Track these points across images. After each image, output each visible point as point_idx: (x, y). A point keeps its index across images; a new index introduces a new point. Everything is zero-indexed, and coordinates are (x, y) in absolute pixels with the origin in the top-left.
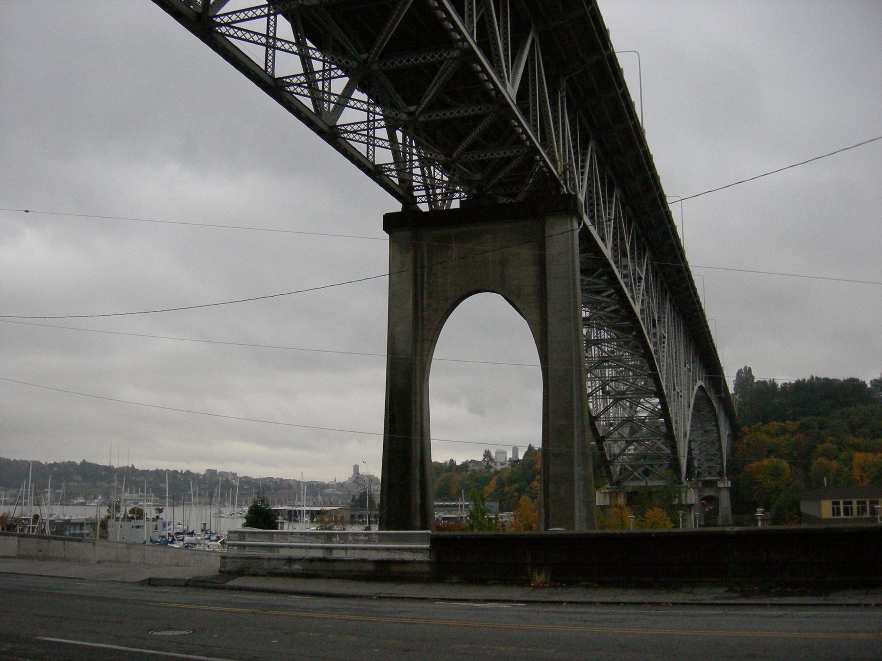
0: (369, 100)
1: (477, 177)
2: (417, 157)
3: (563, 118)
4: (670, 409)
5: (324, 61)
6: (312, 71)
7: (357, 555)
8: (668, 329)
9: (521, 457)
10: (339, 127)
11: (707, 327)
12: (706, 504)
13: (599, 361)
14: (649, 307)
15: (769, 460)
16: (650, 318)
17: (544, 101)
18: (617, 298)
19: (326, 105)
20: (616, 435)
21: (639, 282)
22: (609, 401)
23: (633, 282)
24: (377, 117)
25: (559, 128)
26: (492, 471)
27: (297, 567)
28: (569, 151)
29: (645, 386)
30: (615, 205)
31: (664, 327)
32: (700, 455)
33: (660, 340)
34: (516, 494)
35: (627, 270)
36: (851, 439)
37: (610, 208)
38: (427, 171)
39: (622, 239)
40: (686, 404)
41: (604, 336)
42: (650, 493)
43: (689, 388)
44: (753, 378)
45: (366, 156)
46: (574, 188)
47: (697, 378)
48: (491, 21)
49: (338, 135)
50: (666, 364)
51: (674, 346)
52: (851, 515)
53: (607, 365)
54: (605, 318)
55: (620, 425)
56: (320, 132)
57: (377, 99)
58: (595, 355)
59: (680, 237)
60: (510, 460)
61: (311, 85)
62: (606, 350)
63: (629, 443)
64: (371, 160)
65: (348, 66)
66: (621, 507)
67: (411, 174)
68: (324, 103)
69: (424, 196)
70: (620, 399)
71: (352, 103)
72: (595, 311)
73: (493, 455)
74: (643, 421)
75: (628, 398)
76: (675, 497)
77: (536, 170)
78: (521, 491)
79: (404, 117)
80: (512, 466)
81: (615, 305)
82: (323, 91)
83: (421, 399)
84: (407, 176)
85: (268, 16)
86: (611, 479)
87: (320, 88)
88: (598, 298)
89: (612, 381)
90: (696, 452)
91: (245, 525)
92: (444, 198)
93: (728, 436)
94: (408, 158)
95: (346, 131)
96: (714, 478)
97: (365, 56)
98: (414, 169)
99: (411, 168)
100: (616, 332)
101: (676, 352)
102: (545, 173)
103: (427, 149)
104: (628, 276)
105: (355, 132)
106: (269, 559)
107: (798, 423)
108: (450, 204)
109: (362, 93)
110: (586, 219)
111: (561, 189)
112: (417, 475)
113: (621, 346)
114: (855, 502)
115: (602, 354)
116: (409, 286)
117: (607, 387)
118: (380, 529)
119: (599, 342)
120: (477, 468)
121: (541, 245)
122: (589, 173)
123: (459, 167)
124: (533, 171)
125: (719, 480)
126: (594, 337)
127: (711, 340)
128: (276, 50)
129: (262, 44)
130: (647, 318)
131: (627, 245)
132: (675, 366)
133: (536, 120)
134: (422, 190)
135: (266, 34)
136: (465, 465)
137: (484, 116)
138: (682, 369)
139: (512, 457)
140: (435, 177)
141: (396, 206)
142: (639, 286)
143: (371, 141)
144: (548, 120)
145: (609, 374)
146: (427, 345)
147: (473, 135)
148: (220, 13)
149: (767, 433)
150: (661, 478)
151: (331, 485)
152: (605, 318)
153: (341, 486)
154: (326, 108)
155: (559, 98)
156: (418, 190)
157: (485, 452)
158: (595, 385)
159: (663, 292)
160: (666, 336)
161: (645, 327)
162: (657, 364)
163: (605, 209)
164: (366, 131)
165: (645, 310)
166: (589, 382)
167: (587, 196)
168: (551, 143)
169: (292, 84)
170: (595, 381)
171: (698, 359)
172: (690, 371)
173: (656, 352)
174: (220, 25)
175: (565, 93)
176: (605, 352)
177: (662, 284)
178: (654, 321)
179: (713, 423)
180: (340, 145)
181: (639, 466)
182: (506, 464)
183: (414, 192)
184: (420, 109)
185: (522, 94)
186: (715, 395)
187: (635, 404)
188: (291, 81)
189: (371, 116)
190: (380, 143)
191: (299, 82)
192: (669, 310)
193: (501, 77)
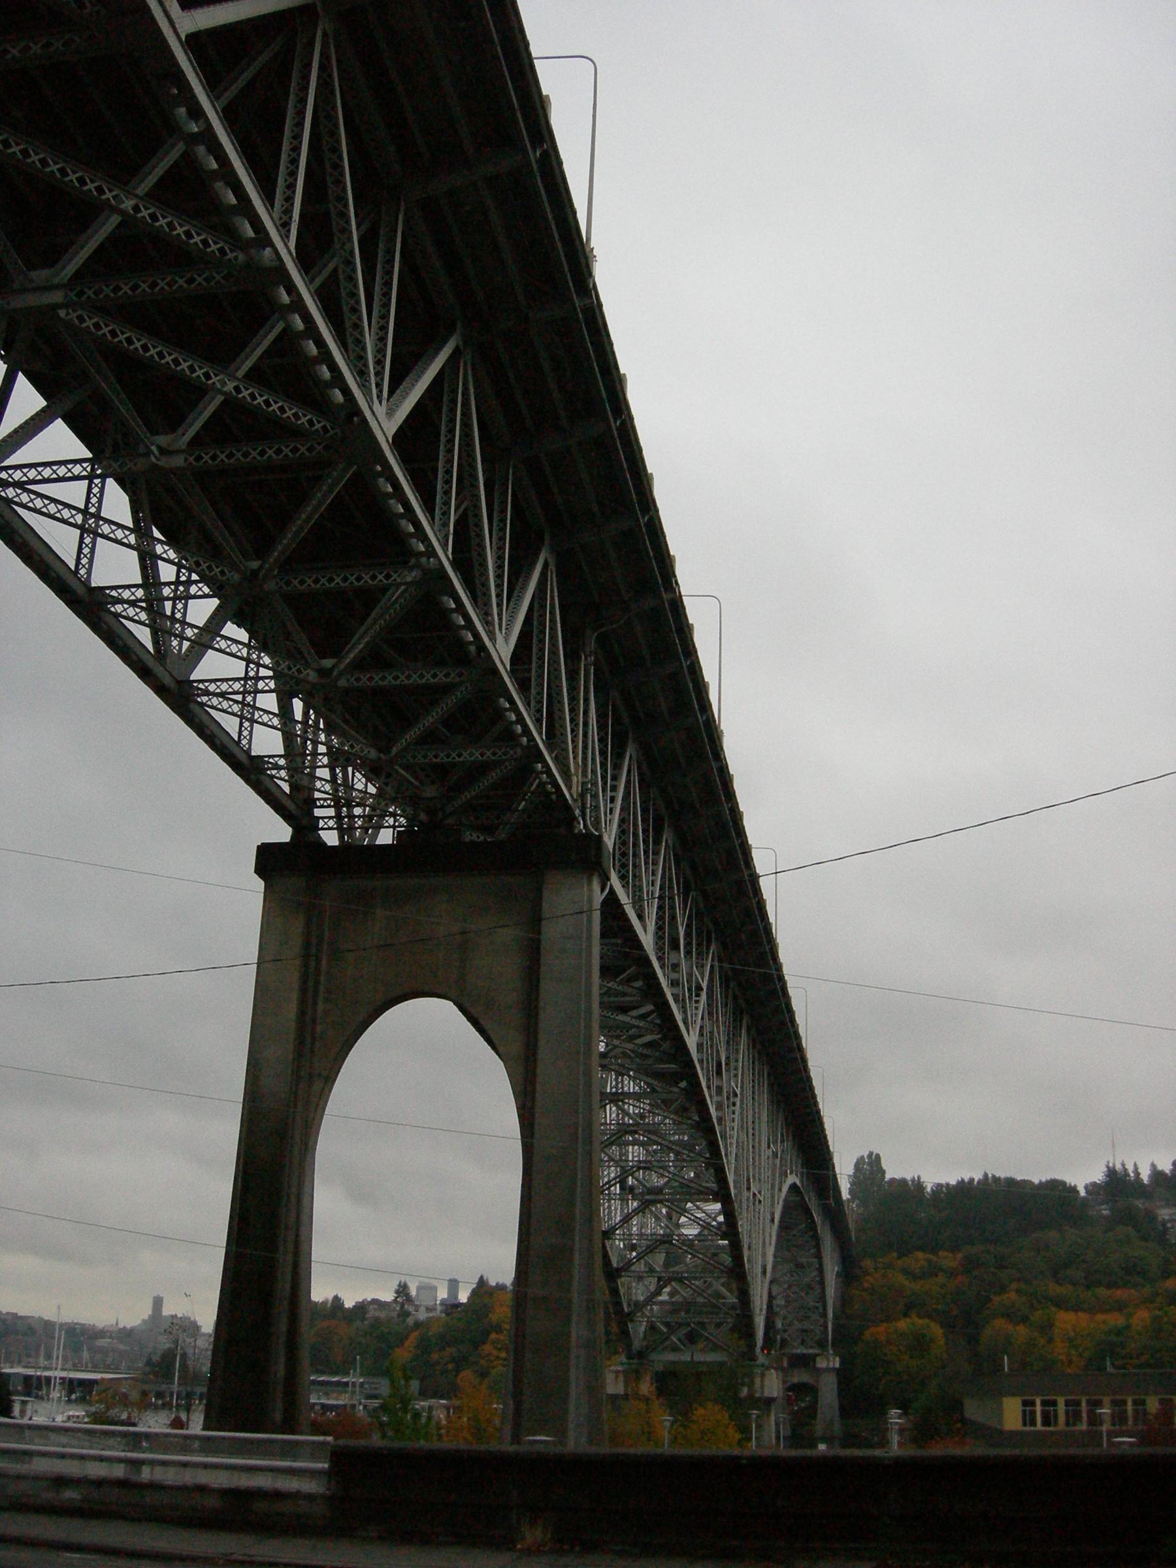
0: (250, 641)
1: (430, 792)
2: (325, 747)
3: (586, 700)
4: (740, 1223)
5: (180, 566)
6: (158, 582)
7: (189, 1477)
8: (742, 1081)
9: (463, 1297)
10: (195, 685)
11: (809, 1079)
12: (793, 1398)
13: (619, 1131)
14: (712, 1039)
15: (908, 1320)
16: (712, 1059)
17: (556, 670)
18: (658, 1021)
19: (175, 643)
20: (640, 1267)
21: (698, 995)
22: (632, 1204)
23: (687, 994)
24: (263, 672)
25: (579, 717)
26: (410, 1321)
27: (71, 1495)
28: (593, 759)
29: (696, 1181)
30: (664, 858)
31: (736, 1076)
32: (786, 1307)
33: (728, 1098)
34: (450, 1366)
35: (679, 972)
36: (1055, 1289)
37: (655, 863)
38: (340, 775)
39: (673, 918)
40: (769, 1217)
41: (629, 1088)
42: (698, 1376)
43: (773, 1186)
44: (883, 1172)
45: (236, 739)
46: (597, 823)
47: (789, 1171)
48: (479, 525)
49: (191, 698)
50: (737, 1142)
51: (750, 1112)
52: (1054, 1426)
53: (631, 1138)
54: (633, 1055)
55: (651, 1249)
56: (161, 690)
57: (262, 640)
58: (611, 1120)
59: (772, 919)
60: (443, 1302)
61: (152, 605)
62: (631, 1111)
63: (662, 1282)
64: (244, 746)
65: (224, 578)
66: (646, 1400)
67: (313, 777)
68: (173, 638)
69: (330, 818)
70: (654, 1202)
71: (223, 644)
72: (616, 1042)
73: (413, 1292)
74: (688, 1243)
75: (667, 1200)
76: (743, 1384)
77: (532, 789)
78: (461, 1362)
79: (312, 676)
80: (448, 1314)
81: (652, 1032)
82: (172, 618)
83: (299, 1185)
84: (305, 782)
85: (90, 478)
86: (629, 1346)
87: (169, 613)
88: (621, 1018)
89: (639, 1168)
90: (779, 1301)
91: (204, 1429)
92: (366, 825)
93: (838, 1275)
94: (310, 748)
95: (207, 693)
96: (811, 1351)
97: (255, 564)
98: (317, 770)
99: (314, 767)
100: (649, 1080)
101: (753, 1122)
102: (548, 794)
103: (342, 735)
104: (678, 984)
105: (223, 695)
106: (19, 1477)
107: (960, 1256)
108: (375, 836)
109: (239, 626)
110: (615, 881)
111: (576, 823)
112: (283, 1326)
113: (657, 1107)
114: (1061, 1402)
115: (623, 1118)
116: (293, 977)
117: (630, 1178)
118: (206, 1427)
119: (621, 1097)
120: (382, 1315)
121: (535, 921)
122: (623, 800)
123: (397, 772)
124: (525, 788)
125: (818, 1355)
126: (611, 1088)
127: (816, 1104)
128: (99, 539)
129: (75, 526)
130: (707, 1059)
131: (680, 928)
132: (751, 1147)
133: (541, 702)
134: (329, 806)
135: (83, 507)
136: (361, 1307)
137: (447, 689)
138: (762, 1154)
139: (446, 1296)
140: (353, 785)
141: (281, 832)
142: (697, 1002)
143: (248, 713)
144: (561, 702)
145: (633, 1156)
146: (317, 1086)
147: (429, 720)
148: (6, 463)
149: (906, 1272)
150: (716, 1348)
151: (108, 1331)
152: (633, 1055)
153: (127, 1334)
154: (174, 648)
155: (583, 666)
156: (322, 806)
157: (399, 1285)
158: (609, 1174)
159: (737, 1015)
161: (703, 1075)
162: (721, 1143)
163: (646, 863)
164: (241, 696)
165: (705, 1046)
167: (617, 838)
168: (563, 742)
169: (121, 601)
170: (609, 1167)
171: (790, 1134)
172: (777, 1157)
173: (720, 1120)
175: (593, 658)
176: (628, 1114)
177: (735, 998)
178: (719, 1065)
179: (812, 1251)
180: (190, 711)
181: (680, 1325)
182: (435, 1309)
183: (315, 810)
184: (342, 666)
185: (521, 655)
187: (677, 1212)
188: (120, 594)
189: (252, 669)
190: (265, 718)
191: (133, 598)
192: (746, 1046)
193: (487, 623)
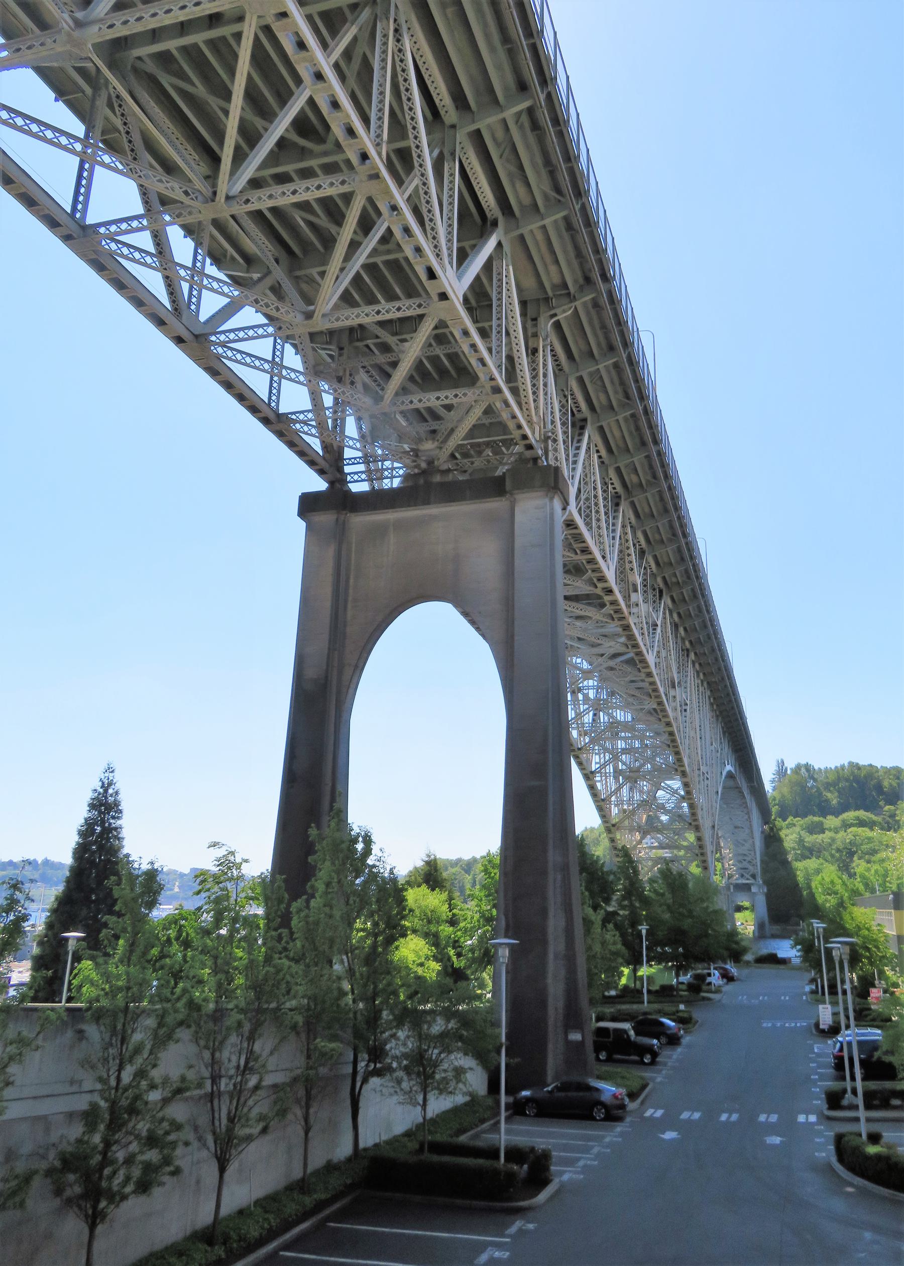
10: (102, 230)
21: (655, 629)
69: (362, 472)
95: (295, 422)
134: (359, 463)
135: (270, 359)
141: (319, 484)
160: (688, 702)
166: (597, 757)
174: (295, 422)
177: (683, 639)
186: (457, 349)
